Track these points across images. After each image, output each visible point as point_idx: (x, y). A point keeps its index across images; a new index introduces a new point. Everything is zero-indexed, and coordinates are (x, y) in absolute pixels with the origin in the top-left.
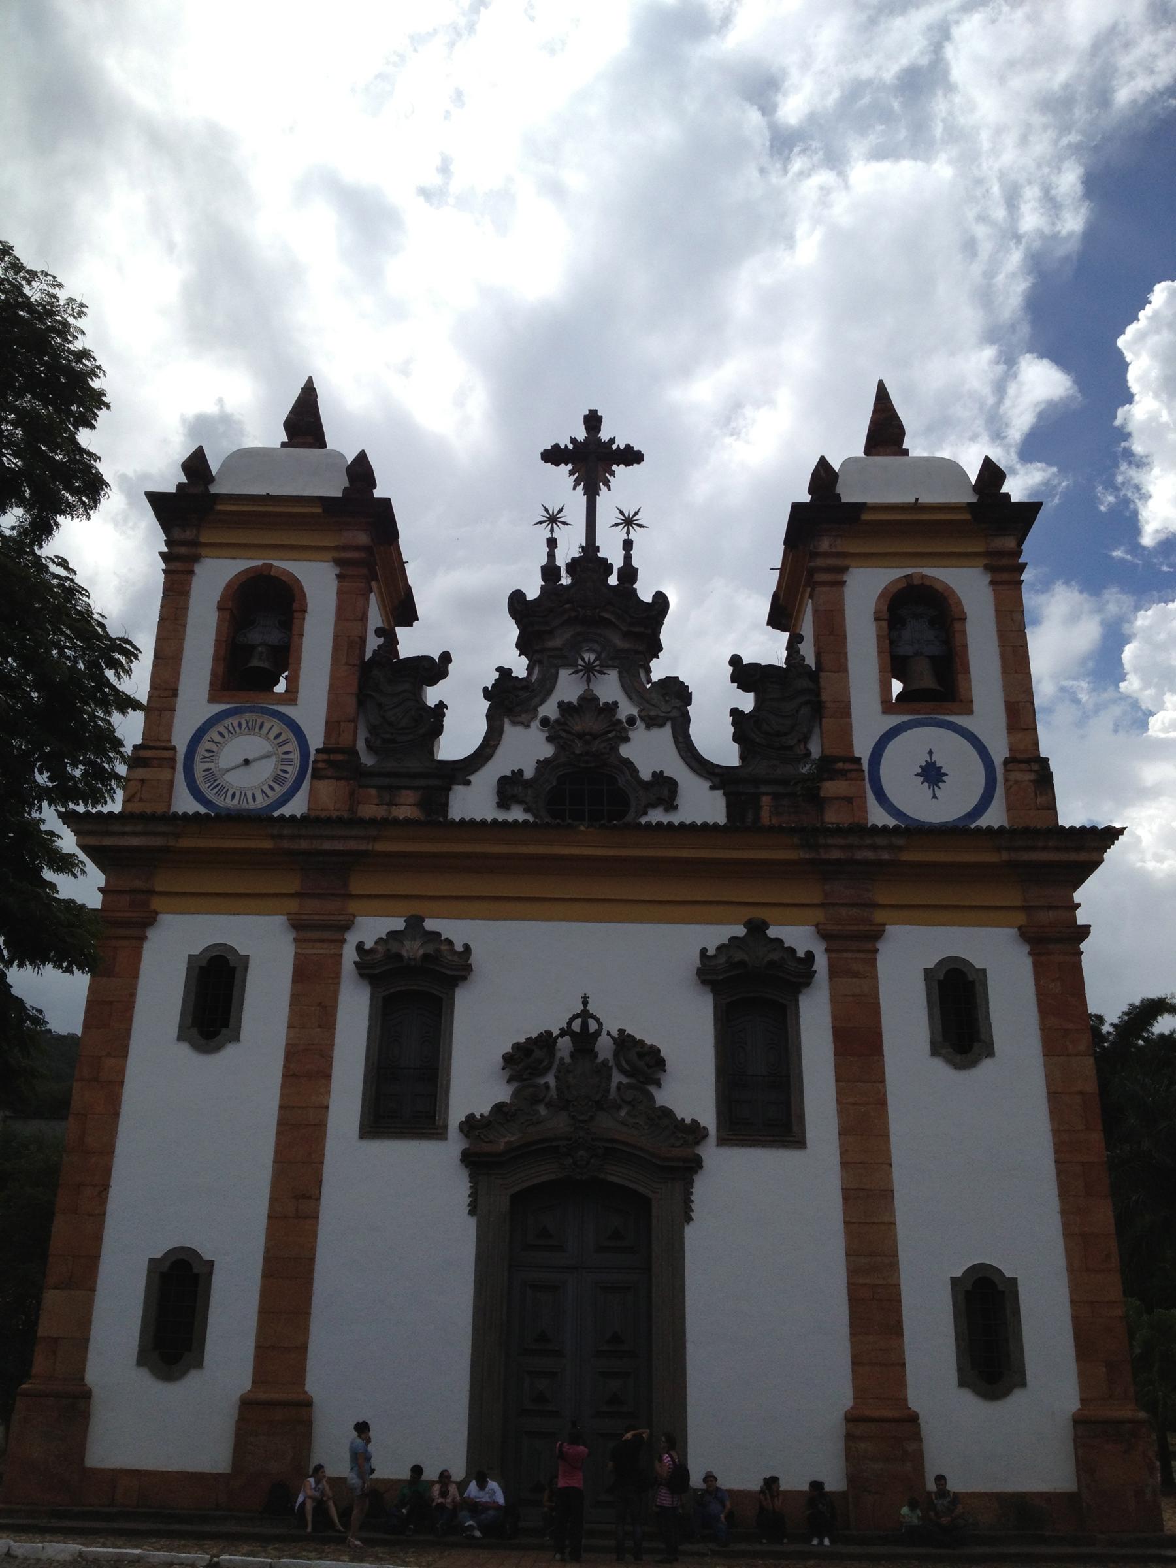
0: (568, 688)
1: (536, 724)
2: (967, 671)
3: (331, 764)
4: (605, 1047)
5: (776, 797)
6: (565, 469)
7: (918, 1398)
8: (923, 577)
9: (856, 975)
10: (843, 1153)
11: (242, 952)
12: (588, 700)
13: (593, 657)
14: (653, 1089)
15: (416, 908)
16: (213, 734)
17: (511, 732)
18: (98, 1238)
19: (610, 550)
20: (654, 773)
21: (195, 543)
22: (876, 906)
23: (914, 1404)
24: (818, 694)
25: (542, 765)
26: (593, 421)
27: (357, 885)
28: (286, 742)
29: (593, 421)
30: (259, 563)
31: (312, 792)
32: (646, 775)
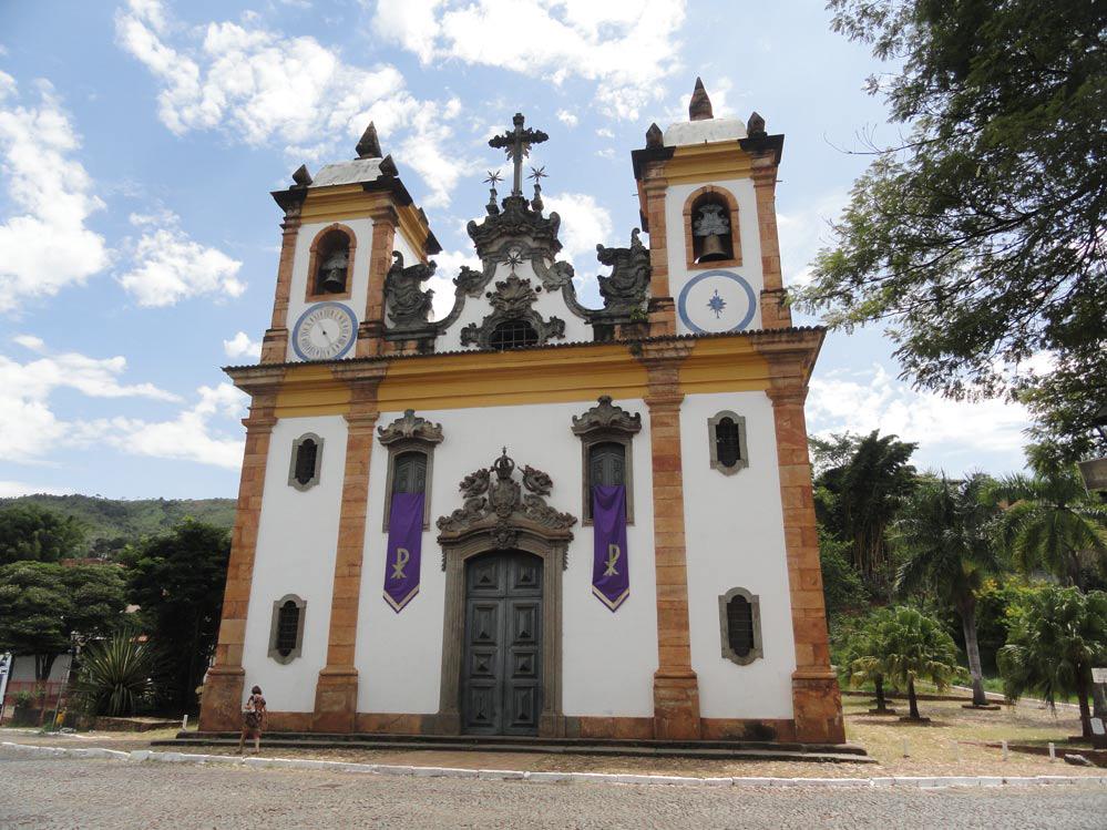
0: (502, 273)
1: (484, 295)
2: (739, 241)
3: (368, 330)
4: (517, 476)
5: (623, 325)
6: (503, 149)
7: (697, 664)
8: (712, 187)
9: (667, 425)
10: (656, 527)
11: (321, 437)
12: (513, 280)
13: (515, 254)
14: (545, 498)
15: (410, 406)
16: (307, 320)
17: (470, 302)
18: (248, 592)
19: (528, 195)
21: (298, 218)
22: (679, 384)
23: (695, 668)
24: (649, 263)
25: (487, 319)
28: (345, 320)
30: (331, 224)
31: (357, 345)
32: (546, 320)
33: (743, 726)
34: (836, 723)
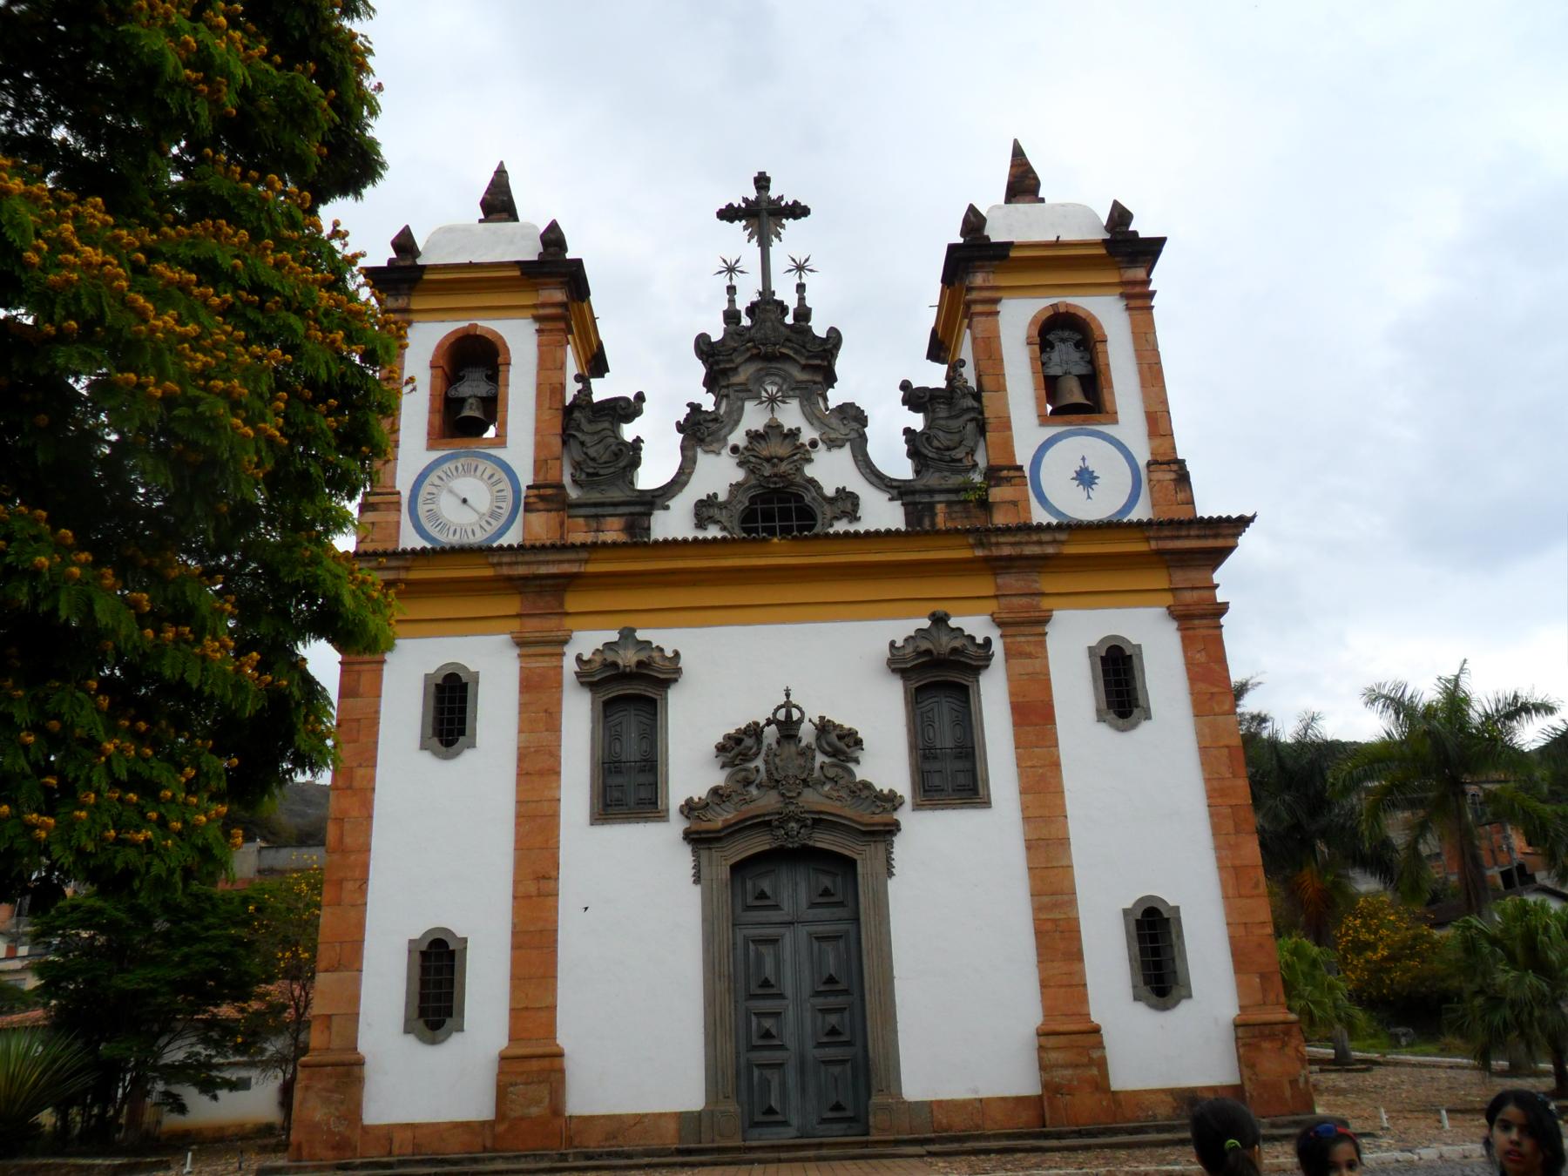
1: (726, 452)
4: (807, 733)
8: (1067, 305)
14: (852, 765)
20: (838, 490)
26: (762, 182)
27: (573, 603)
29: (762, 182)
32: (829, 491)
33: (1170, 1099)
34: (1301, 1085)
